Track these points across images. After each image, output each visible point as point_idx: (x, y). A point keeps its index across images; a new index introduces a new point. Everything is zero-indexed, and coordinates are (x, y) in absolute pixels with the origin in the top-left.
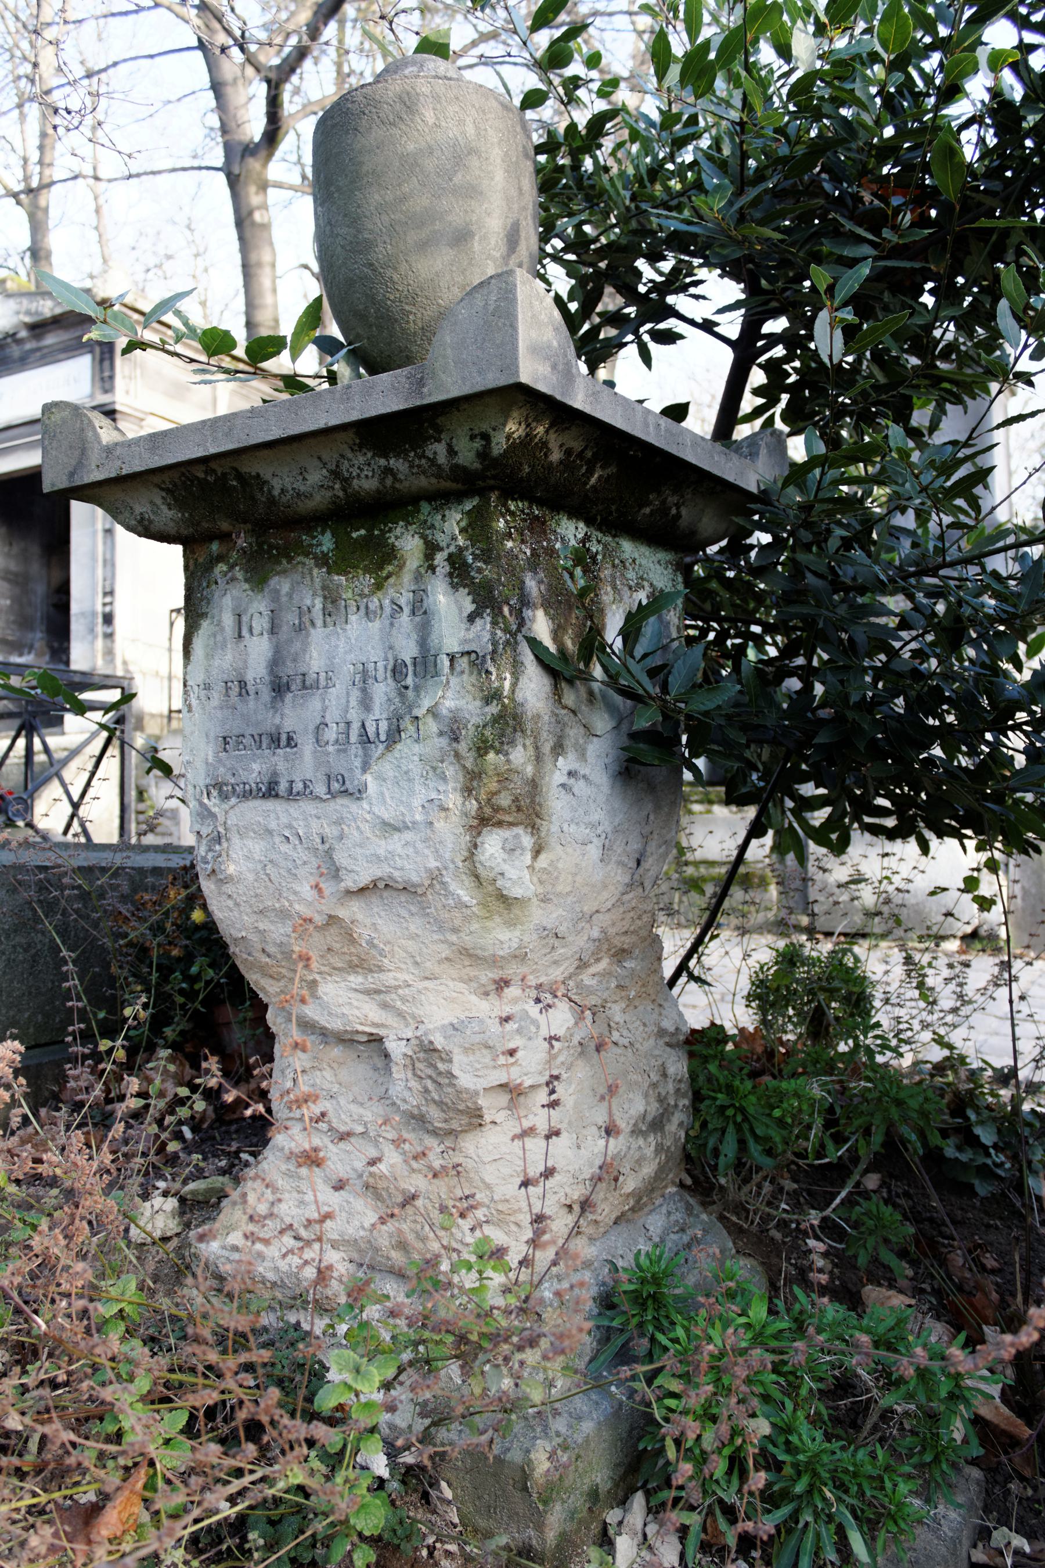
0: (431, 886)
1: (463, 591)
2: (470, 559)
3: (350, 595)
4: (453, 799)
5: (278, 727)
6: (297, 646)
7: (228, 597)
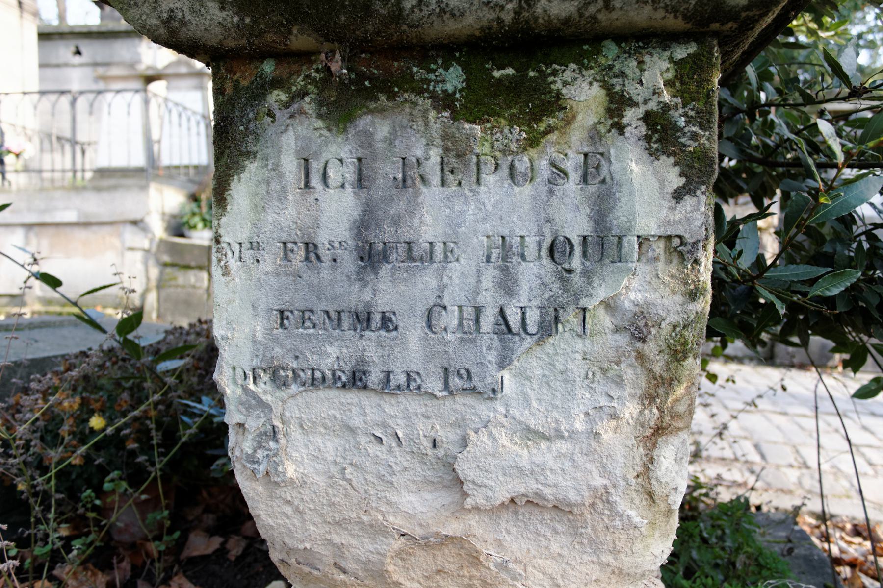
0: (593, 505)
1: (666, 161)
2: (682, 122)
3: (486, 149)
4: (630, 410)
5: (368, 305)
6: (400, 206)
7: (291, 133)
